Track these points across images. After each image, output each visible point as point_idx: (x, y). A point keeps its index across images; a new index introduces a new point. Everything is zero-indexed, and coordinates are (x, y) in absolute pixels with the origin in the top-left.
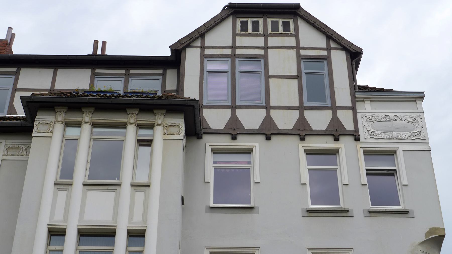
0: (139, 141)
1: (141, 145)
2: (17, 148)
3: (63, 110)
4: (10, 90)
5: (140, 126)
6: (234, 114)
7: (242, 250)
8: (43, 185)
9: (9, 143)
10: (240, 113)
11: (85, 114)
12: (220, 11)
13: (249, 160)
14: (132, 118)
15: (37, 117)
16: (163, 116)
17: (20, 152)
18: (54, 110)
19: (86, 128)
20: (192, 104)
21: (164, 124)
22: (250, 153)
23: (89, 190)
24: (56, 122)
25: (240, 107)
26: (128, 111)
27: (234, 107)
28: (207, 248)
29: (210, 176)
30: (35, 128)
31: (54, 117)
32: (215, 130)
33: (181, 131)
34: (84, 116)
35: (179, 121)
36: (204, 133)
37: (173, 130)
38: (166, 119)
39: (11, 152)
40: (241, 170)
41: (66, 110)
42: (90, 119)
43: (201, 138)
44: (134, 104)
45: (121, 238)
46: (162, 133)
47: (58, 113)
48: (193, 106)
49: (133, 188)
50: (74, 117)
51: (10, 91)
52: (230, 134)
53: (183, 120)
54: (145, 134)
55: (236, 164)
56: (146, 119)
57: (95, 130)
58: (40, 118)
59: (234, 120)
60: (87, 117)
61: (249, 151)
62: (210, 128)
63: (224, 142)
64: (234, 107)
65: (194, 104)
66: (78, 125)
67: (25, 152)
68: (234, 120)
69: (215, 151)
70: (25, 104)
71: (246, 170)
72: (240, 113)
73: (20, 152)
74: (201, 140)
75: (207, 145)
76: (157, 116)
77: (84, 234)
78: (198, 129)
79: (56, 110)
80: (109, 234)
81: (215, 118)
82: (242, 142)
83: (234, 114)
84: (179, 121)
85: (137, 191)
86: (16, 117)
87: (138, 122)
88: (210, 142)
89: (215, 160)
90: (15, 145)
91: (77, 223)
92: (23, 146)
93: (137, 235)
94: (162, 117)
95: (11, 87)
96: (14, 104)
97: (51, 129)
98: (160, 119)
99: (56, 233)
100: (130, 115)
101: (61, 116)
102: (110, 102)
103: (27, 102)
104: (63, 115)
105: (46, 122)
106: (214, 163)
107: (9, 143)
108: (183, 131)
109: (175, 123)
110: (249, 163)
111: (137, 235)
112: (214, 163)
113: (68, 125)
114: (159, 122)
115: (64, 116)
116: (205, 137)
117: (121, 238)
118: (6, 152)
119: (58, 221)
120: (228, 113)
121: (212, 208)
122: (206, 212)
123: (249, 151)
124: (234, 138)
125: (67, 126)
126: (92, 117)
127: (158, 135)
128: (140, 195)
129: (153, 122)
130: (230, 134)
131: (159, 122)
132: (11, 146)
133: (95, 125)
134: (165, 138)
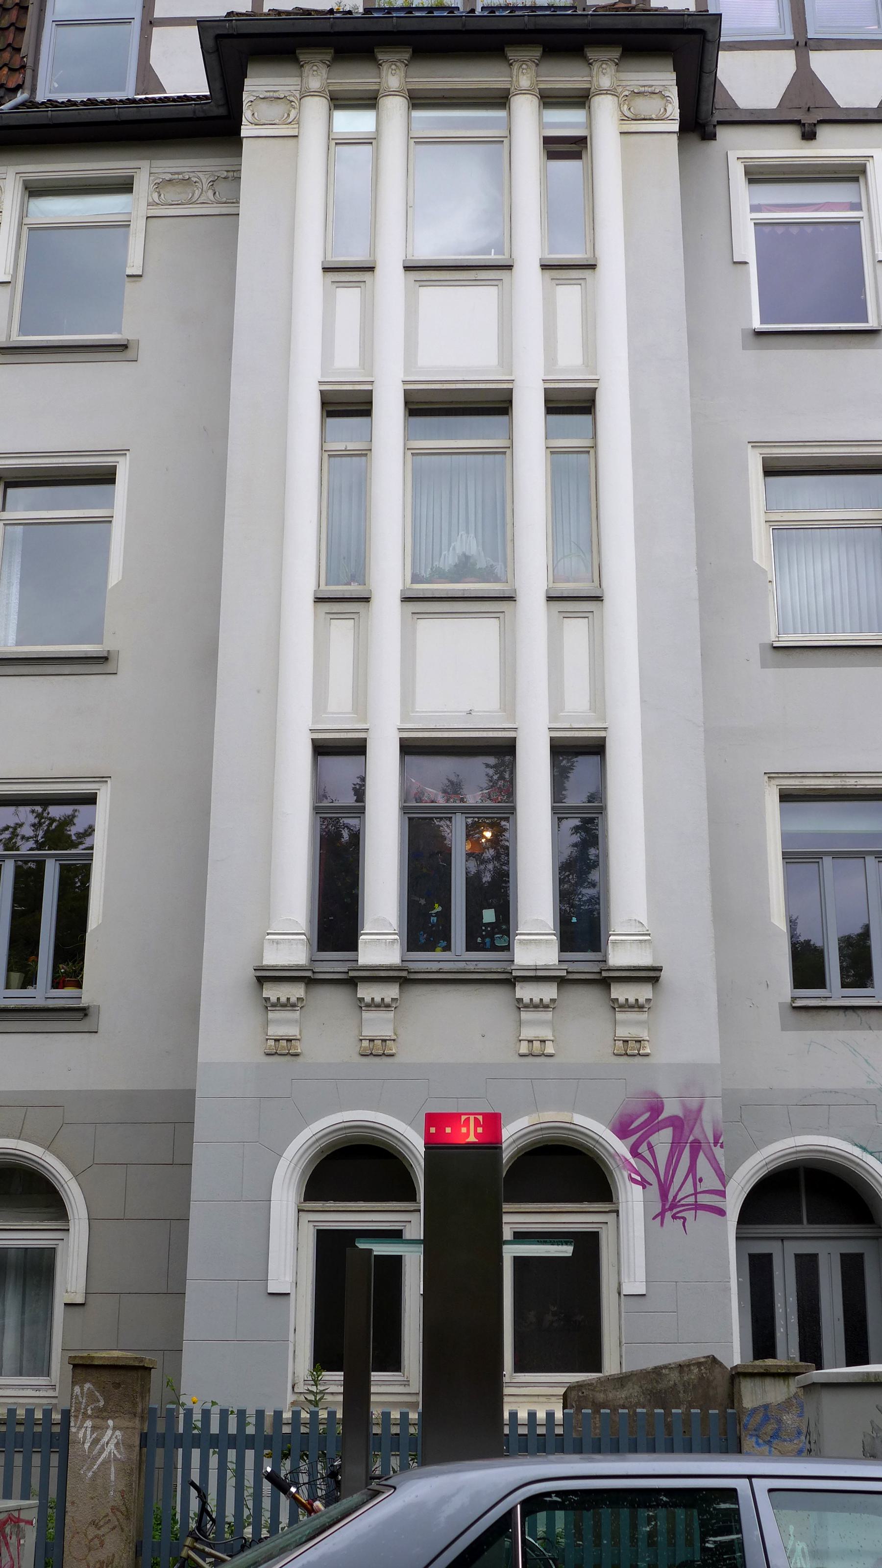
0: (548, 141)
1: (552, 155)
2: (187, 182)
3: (321, 57)
4: (136, 25)
5: (550, 100)
6: (803, 64)
7: (854, 450)
8: (292, 273)
9: (160, 170)
10: (821, 63)
11: (385, 66)
12: (289, 8)
13: (855, 200)
14: (524, 76)
15: (247, 81)
16: (614, 68)
17: (197, 193)
18: (296, 60)
19: (394, 107)
20: (699, 26)
21: (620, 89)
22: (856, 180)
23: (422, 283)
24: (305, 94)
25: (822, 45)
26: (511, 54)
27: (802, 45)
28: (755, 444)
29: (746, 246)
30: (247, 114)
31: (296, 80)
32: (752, 112)
33: (669, 108)
34: (384, 73)
35: (663, 79)
36: (721, 123)
37: (645, 106)
38: (623, 76)
39: (170, 194)
40: (822, 228)
41: (329, 57)
42: (403, 80)
43: (713, 137)
44: (531, 31)
45: (529, 409)
46: (616, 116)
47: (307, 68)
48: (701, 32)
49: (549, 273)
50: (354, 78)
51: (136, 27)
52: (797, 123)
53: (674, 76)
54: (566, 121)
55: (816, 210)
56: (566, 76)
57: (417, 114)
58: (257, 85)
59: (805, 82)
60: (393, 76)
61: (853, 173)
62: (737, 108)
63: (781, 147)
64: (802, 45)
65: (706, 26)
66: (368, 101)
67: (210, 193)
68: (805, 82)
69: (758, 175)
70: (211, 43)
71: (846, 227)
72: (821, 63)
73: (197, 193)
74: (713, 142)
75: (732, 156)
76: (596, 66)
77: (422, 406)
78: (705, 108)
79: (302, 58)
80: (497, 404)
81: (749, 79)
82: (834, 146)
83: (803, 64)
84: (663, 79)
85: (560, 282)
86: (165, 97)
87: (542, 86)
88: (738, 147)
89: (756, 202)
90: (178, 173)
91: (402, 377)
92: (200, 174)
93: (572, 404)
94: (611, 69)
95: (137, 14)
96: (152, 62)
97: (293, 113)
98: (604, 74)
99: (346, 405)
100: (516, 66)
101: (317, 76)
102: (459, 27)
103: (218, 37)
104: (324, 71)
105: (276, 95)
106: (754, 208)
107: (160, 170)
108: (674, 110)
109: (651, 86)
110: (857, 207)
111: (572, 404)
112: (754, 208)
113: (339, 101)
114: (605, 82)
115: (325, 76)
116: (724, 134)
117: (529, 409)
118: (155, 195)
119: (347, 370)
120: (787, 60)
121: (759, 334)
122: (744, 348)
123: (853, 173)
124: (809, 135)
125: (338, 107)
126: (406, 77)
127: (605, 121)
128: (569, 295)
129: (587, 86)
130: (797, 123)
131: (605, 82)
132: (168, 177)
133: (418, 100)
134: (626, 128)
